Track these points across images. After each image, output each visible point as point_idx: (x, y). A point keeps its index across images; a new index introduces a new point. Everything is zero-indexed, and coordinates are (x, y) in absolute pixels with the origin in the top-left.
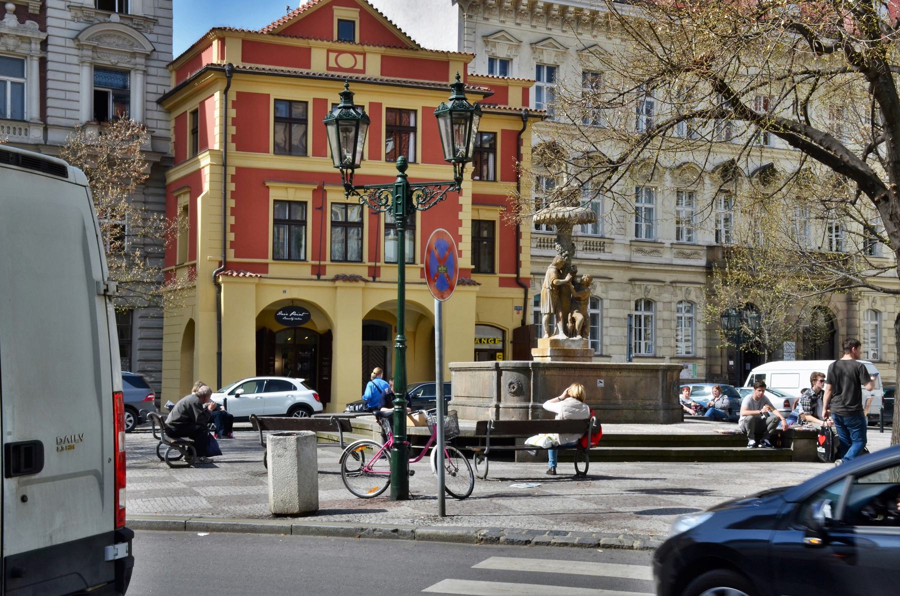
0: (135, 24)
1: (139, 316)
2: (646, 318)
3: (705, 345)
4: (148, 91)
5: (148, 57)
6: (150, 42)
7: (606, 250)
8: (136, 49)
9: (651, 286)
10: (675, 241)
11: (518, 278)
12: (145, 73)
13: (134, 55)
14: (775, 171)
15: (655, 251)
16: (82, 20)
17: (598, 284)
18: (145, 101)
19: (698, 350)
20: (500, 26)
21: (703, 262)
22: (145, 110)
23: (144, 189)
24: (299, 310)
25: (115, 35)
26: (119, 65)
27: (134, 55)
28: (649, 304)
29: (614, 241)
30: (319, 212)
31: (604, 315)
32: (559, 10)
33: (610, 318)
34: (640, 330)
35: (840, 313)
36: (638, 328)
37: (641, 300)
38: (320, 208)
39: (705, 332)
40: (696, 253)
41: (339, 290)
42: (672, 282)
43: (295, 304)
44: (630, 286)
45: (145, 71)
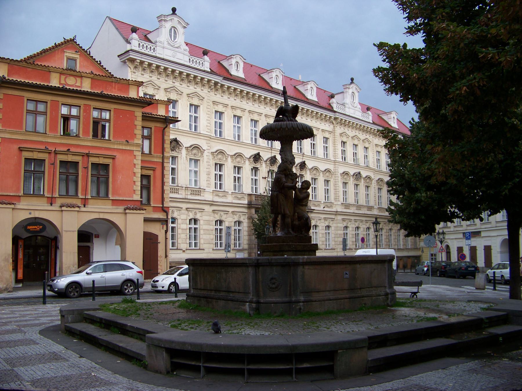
3: (247, 243)
7: (201, 195)
9: (222, 213)
10: (214, 189)
11: (163, 207)
14: (260, 156)
15: (225, 196)
17: (198, 212)
19: (245, 245)
20: (195, 90)
21: (246, 202)
24: (40, 224)
28: (196, 221)
29: (205, 190)
30: (52, 166)
31: (179, 227)
33: (204, 230)
34: (236, 236)
36: (191, 234)
37: (217, 220)
38: (52, 164)
39: (247, 236)
40: (243, 197)
41: (128, 215)
42: (187, 209)
43: (37, 221)
44: (187, 212)
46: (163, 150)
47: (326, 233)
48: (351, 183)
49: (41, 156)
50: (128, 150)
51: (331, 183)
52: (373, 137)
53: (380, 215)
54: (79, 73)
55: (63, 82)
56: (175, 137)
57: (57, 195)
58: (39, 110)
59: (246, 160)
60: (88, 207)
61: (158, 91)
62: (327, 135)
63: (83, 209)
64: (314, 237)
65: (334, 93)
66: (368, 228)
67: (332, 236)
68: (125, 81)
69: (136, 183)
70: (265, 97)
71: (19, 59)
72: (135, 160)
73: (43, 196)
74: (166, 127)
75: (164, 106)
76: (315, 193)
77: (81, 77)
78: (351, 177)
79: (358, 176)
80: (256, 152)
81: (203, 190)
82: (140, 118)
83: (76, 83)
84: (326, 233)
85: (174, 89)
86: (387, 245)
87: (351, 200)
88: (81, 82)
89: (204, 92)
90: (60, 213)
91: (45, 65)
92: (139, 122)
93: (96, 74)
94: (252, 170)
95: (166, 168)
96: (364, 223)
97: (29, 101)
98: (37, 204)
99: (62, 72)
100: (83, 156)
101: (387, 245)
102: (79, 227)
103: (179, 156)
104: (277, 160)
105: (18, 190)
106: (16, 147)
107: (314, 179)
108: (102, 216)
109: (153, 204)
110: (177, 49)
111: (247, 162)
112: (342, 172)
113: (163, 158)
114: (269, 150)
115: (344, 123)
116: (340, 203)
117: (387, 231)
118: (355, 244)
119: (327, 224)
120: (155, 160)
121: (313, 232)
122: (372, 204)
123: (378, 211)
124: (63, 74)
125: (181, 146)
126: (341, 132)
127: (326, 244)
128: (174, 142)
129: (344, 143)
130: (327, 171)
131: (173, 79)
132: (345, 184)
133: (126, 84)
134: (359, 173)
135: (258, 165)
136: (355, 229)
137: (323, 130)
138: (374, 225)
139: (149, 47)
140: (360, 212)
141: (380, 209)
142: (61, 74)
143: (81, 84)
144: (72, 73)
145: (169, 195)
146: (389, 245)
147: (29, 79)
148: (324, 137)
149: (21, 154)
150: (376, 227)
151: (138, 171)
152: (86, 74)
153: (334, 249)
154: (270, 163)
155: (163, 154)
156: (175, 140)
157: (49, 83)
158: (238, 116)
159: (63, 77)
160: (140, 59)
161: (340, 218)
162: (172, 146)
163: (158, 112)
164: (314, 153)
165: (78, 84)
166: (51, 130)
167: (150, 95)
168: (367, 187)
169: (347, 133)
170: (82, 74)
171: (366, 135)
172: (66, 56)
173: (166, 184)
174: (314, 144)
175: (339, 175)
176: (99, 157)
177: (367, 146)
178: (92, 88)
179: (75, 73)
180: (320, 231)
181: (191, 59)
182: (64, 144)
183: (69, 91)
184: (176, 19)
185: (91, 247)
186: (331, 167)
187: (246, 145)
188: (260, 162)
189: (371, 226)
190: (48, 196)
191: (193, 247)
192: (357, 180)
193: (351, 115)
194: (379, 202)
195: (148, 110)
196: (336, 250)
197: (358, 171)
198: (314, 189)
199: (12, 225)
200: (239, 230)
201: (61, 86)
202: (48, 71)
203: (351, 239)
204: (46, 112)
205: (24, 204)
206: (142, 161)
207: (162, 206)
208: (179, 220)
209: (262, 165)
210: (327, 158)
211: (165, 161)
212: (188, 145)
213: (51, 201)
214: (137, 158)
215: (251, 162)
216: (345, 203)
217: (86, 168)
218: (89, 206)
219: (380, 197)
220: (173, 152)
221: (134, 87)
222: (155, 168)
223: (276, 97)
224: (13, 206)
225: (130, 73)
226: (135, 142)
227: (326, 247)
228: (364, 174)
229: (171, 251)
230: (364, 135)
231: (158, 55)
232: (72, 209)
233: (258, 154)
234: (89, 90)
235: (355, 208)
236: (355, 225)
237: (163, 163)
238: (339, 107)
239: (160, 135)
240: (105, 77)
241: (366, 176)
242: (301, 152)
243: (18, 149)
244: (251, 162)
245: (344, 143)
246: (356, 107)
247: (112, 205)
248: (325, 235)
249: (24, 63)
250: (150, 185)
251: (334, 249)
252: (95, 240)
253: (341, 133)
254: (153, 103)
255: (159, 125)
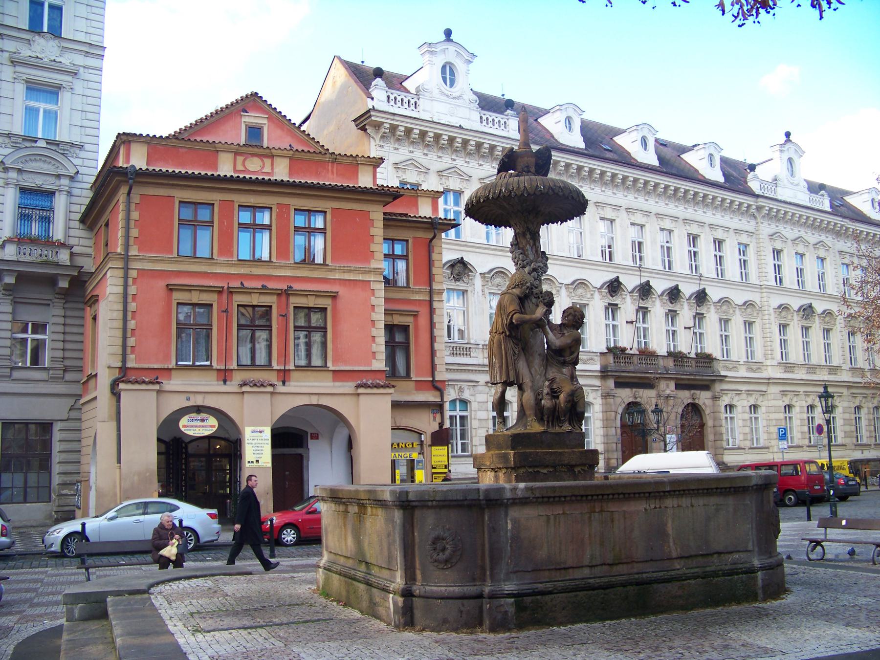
0: (61, 149)
1: (58, 429)
2: (462, 417)
3: (603, 441)
4: (72, 210)
5: (72, 178)
6: (75, 166)
7: (472, 355)
8: (63, 172)
11: (433, 381)
12: (69, 194)
13: (59, 176)
16: (9, 146)
17: (466, 388)
18: (68, 220)
21: (597, 367)
22: (68, 228)
23: (64, 304)
25: (40, 159)
26: (44, 186)
27: (59, 176)
31: (473, 417)
32: (476, 146)
35: (708, 408)
39: (602, 429)
40: (592, 359)
45: (68, 192)
46: (430, 279)
47: (786, 417)
48: (818, 328)
49: (205, 298)
50: (360, 280)
51: (757, 328)
52: (833, 239)
53: (854, 383)
54: (268, 151)
55: (240, 167)
56: (460, 257)
57: (234, 366)
58: (200, 218)
59: (561, 287)
60: (289, 386)
61: (427, 175)
62: (744, 239)
63: (281, 388)
64: (458, 428)
65: (755, 163)
66: (811, 407)
67: (762, 423)
68: (345, 158)
69: (377, 340)
70: (634, 178)
71: (164, 135)
72: (373, 298)
73: (209, 368)
74: (434, 237)
75: (429, 200)
76: (751, 347)
77: (272, 157)
78: (795, 313)
79: (807, 311)
80: (612, 276)
81: (475, 346)
82: (380, 224)
83: (263, 167)
84: (786, 417)
85: (454, 170)
86: (871, 437)
87: (796, 355)
88: (272, 164)
89: (829, 239)
90: (354, 398)
91: (208, 141)
92: (378, 230)
93: (297, 150)
94: (667, 315)
95: (437, 311)
96: (744, 396)
97: (182, 205)
98: (199, 383)
99: (238, 151)
100: (279, 295)
101: (871, 437)
102: (274, 421)
103: (469, 289)
104: (621, 284)
105: (167, 358)
106: (162, 284)
107: (749, 324)
108: (314, 400)
109: (416, 377)
110: (457, 101)
111: (597, 295)
112: (776, 305)
113: (431, 292)
114: (637, 271)
115: (773, 217)
116: (775, 362)
117: (869, 411)
118: (808, 437)
119: (752, 402)
120: (417, 298)
121: (726, 418)
122: (836, 362)
123: (850, 374)
124: (241, 154)
125: (472, 272)
126: (772, 232)
127: (753, 438)
128: (459, 265)
129: (777, 253)
130: (748, 304)
131: (479, 159)
132: (783, 327)
133: (353, 163)
134: (810, 306)
135: (617, 300)
136: (853, 410)
137: (737, 231)
138: (823, 399)
139: (399, 98)
140: (815, 377)
141: (854, 370)
142: (237, 154)
143: (272, 169)
144: (256, 150)
145: (444, 357)
146: (876, 437)
147: (183, 166)
148: (739, 244)
149: (171, 296)
150: (826, 403)
151: (380, 318)
152: (279, 151)
153: (768, 448)
154: (640, 296)
155: (430, 285)
156: (461, 261)
157: (217, 171)
158: (455, 192)
159: (240, 159)
160: (391, 122)
161: (774, 390)
162: (456, 272)
163: (418, 209)
164: (721, 273)
165: (267, 169)
166: (221, 252)
167: (411, 184)
168: (827, 331)
169: (783, 233)
170: (273, 151)
171: (820, 236)
172: (245, 122)
173: (438, 340)
174: (720, 257)
175: (772, 311)
176: (307, 295)
177: (822, 256)
178: (291, 174)
179: (260, 151)
180: (740, 416)
181: (391, 95)
182: (244, 274)
183: (250, 181)
184: (451, 48)
185: (305, 455)
186: (755, 297)
187: (683, 277)
188: (621, 294)
189: (817, 402)
190: (219, 367)
191: (460, 452)
192: (806, 319)
193: (789, 200)
194: (851, 358)
195: (396, 208)
196: (771, 450)
197: (806, 302)
198: (673, 334)
199: (158, 421)
200: (462, 418)
201: (235, 175)
202: (213, 151)
203: (741, 430)
204: (212, 222)
205: (175, 383)
206: (387, 300)
207: (431, 379)
208: (473, 403)
209: (624, 299)
210: (722, 277)
211: (435, 298)
212: (486, 270)
213: (225, 375)
214: (377, 295)
215: (665, 301)
216: (784, 361)
217: (285, 316)
218: (292, 383)
219: (852, 349)
220: (458, 283)
221: (366, 168)
222: (417, 312)
223: (424, 126)
224: (157, 387)
225: (374, 147)
226: (372, 266)
227: (753, 444)
228: (819, 307)
229: (454, 459)
230: (816, 235)
231: (779, 198)
232: (262, 389)
233: (617, 279)
234: (286, 179)
235: (804, 371)
236: (806, 402)
237: (431, 302)
238: (769, 187)
239: (424, 253)
240: (314, 155)
241: (824, 311)
242: (696, 273)
243: (165, 288)
244: (665, 301)
245: (777, 253)
246: (457, 98)
247: (334, 380)
248: (749, 421)
249: (174, 140)
250: (409, 343)
251: (768, 448)
252: (311, 443)
253: (770, 234)
254: (402, 195)
255: (421, 234)
